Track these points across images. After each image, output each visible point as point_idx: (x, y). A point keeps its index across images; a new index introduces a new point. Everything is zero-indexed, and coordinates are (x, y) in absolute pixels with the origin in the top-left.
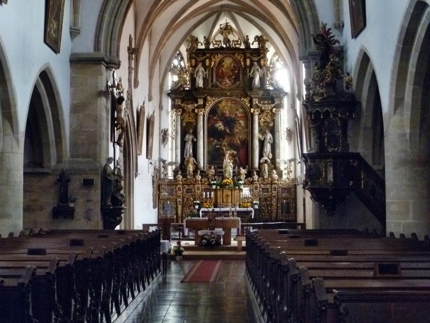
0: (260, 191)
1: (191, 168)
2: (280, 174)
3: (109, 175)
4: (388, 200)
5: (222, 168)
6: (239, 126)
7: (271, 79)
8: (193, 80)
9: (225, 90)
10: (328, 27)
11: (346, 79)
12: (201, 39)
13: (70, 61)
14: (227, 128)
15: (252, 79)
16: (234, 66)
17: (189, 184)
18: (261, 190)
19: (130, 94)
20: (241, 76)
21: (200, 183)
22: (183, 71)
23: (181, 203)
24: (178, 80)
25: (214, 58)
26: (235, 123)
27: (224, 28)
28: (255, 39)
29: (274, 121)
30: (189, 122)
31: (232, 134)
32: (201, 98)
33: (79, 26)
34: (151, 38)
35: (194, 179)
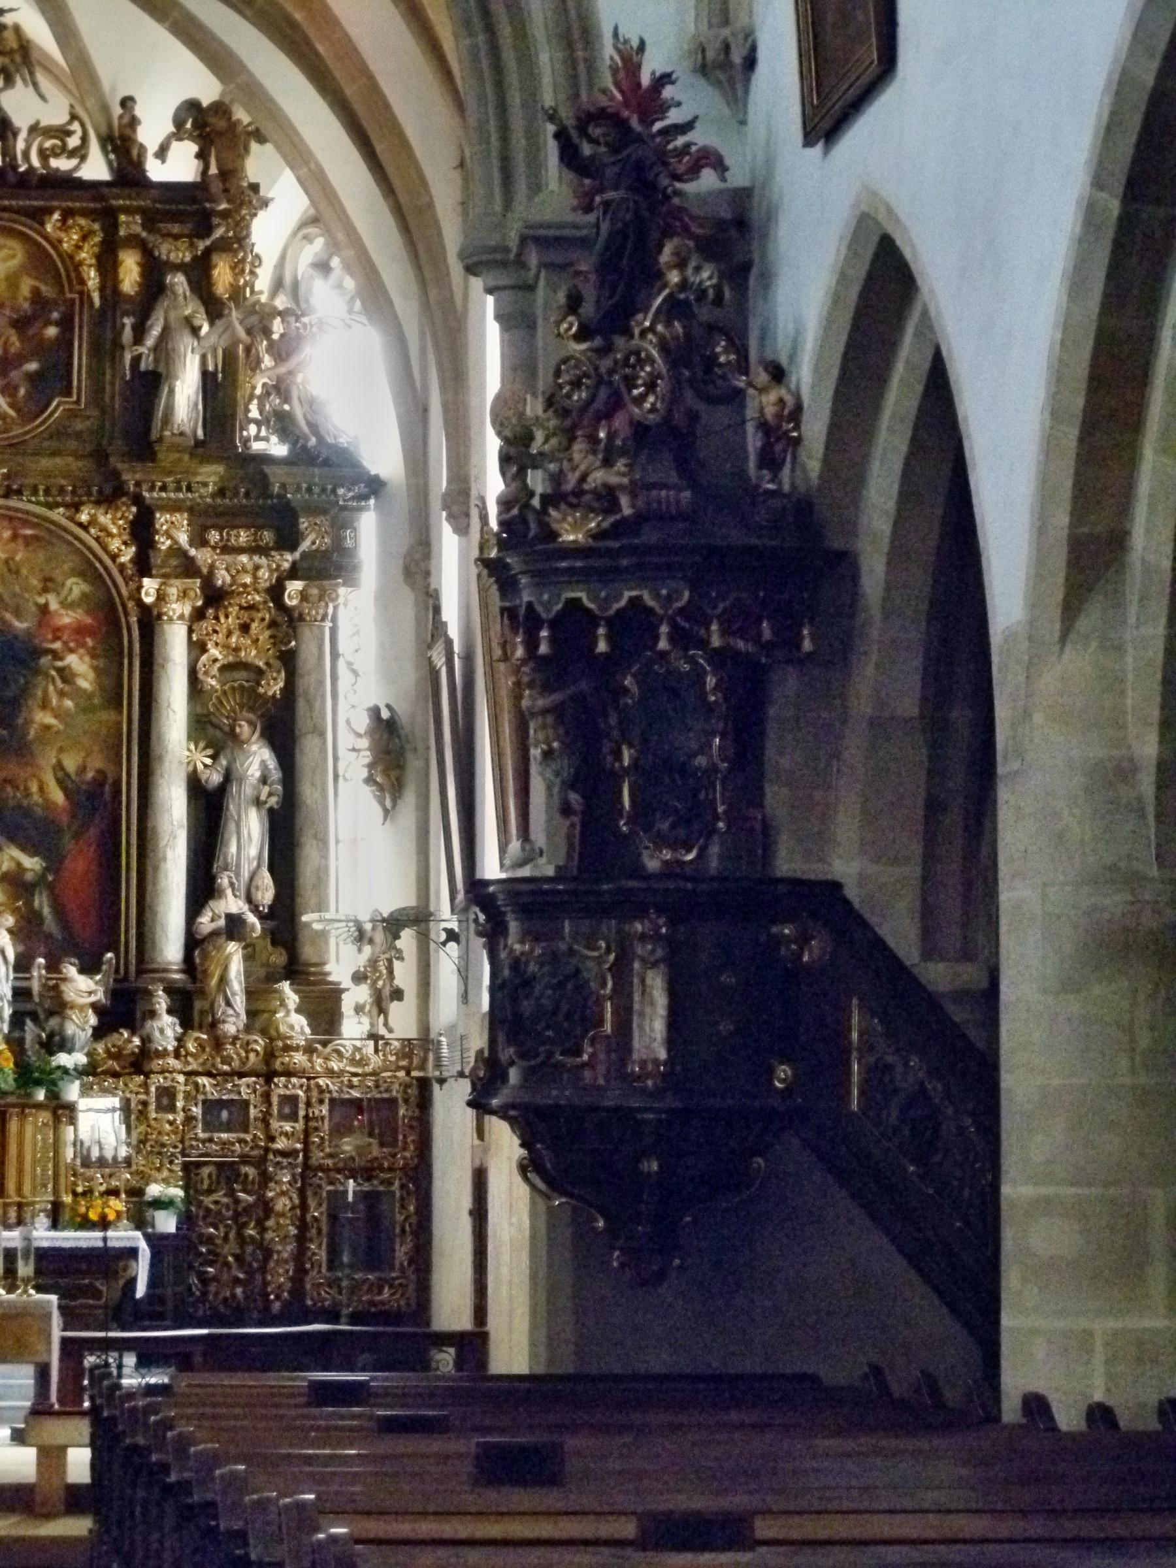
0: (189, 1119)
2: (324, 1010)
4: (1015, 1190)
6: (62, 694)
7: (280, 388)
10: (652, 66)
11: (764, 402)
15: (151, 384)
16: (36, 292)
18: (197, 1111)
20: (80, 359)
26: (37, 672)
28: (179, 123)
29: (289, 660)
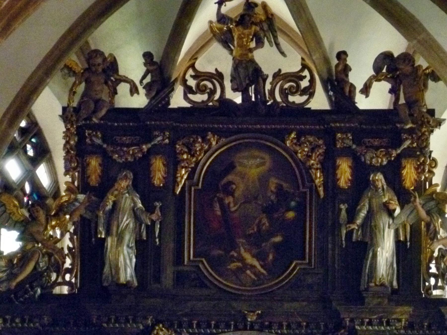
8: (91, 252)
9: (236, 297)
12: (133, 66)
15: (364, 248)
16: (279, 188)
22: (47, 210)
24: (23, 250)
27: (234, 15)
28: (377, 68)
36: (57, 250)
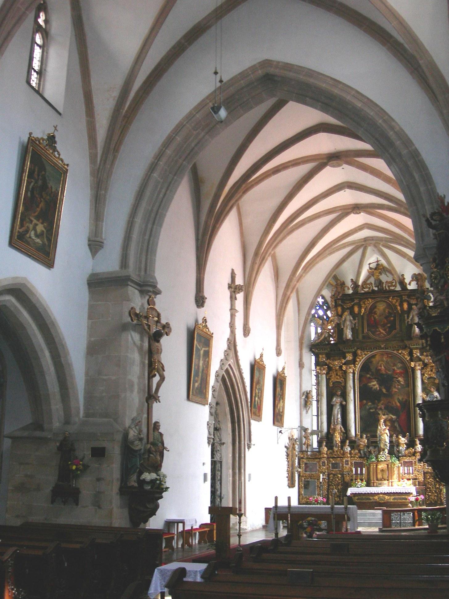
1: (338, 438)
3: (132, 443)
5: (376, 436)
6: (398, 385)
8: (339, 330)
9: (379, 341)
13: (88, 284)
14: (383, 387)
17: (335, 459)
19: (232, 342)
21: (349, 456)
23: (327, 481)
25: (364, 303)
28: (412, 278)
30: (337, 382)
31: (389, 395)
32: (349, 352)
33: (103, 238)
34: (277, 279)
35: (342, 451)
36: (201, 295)
